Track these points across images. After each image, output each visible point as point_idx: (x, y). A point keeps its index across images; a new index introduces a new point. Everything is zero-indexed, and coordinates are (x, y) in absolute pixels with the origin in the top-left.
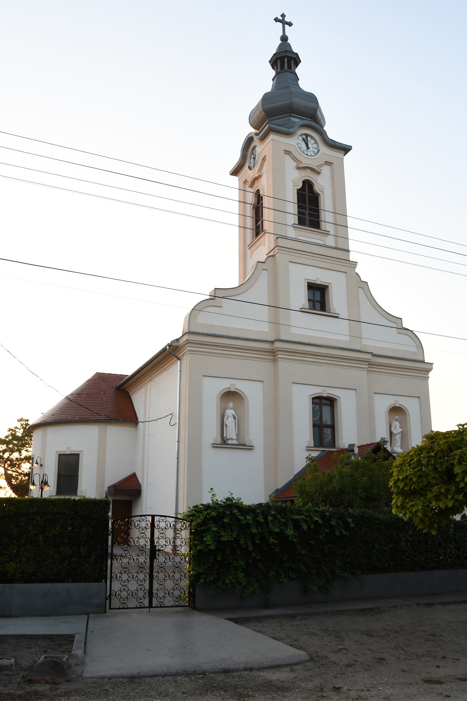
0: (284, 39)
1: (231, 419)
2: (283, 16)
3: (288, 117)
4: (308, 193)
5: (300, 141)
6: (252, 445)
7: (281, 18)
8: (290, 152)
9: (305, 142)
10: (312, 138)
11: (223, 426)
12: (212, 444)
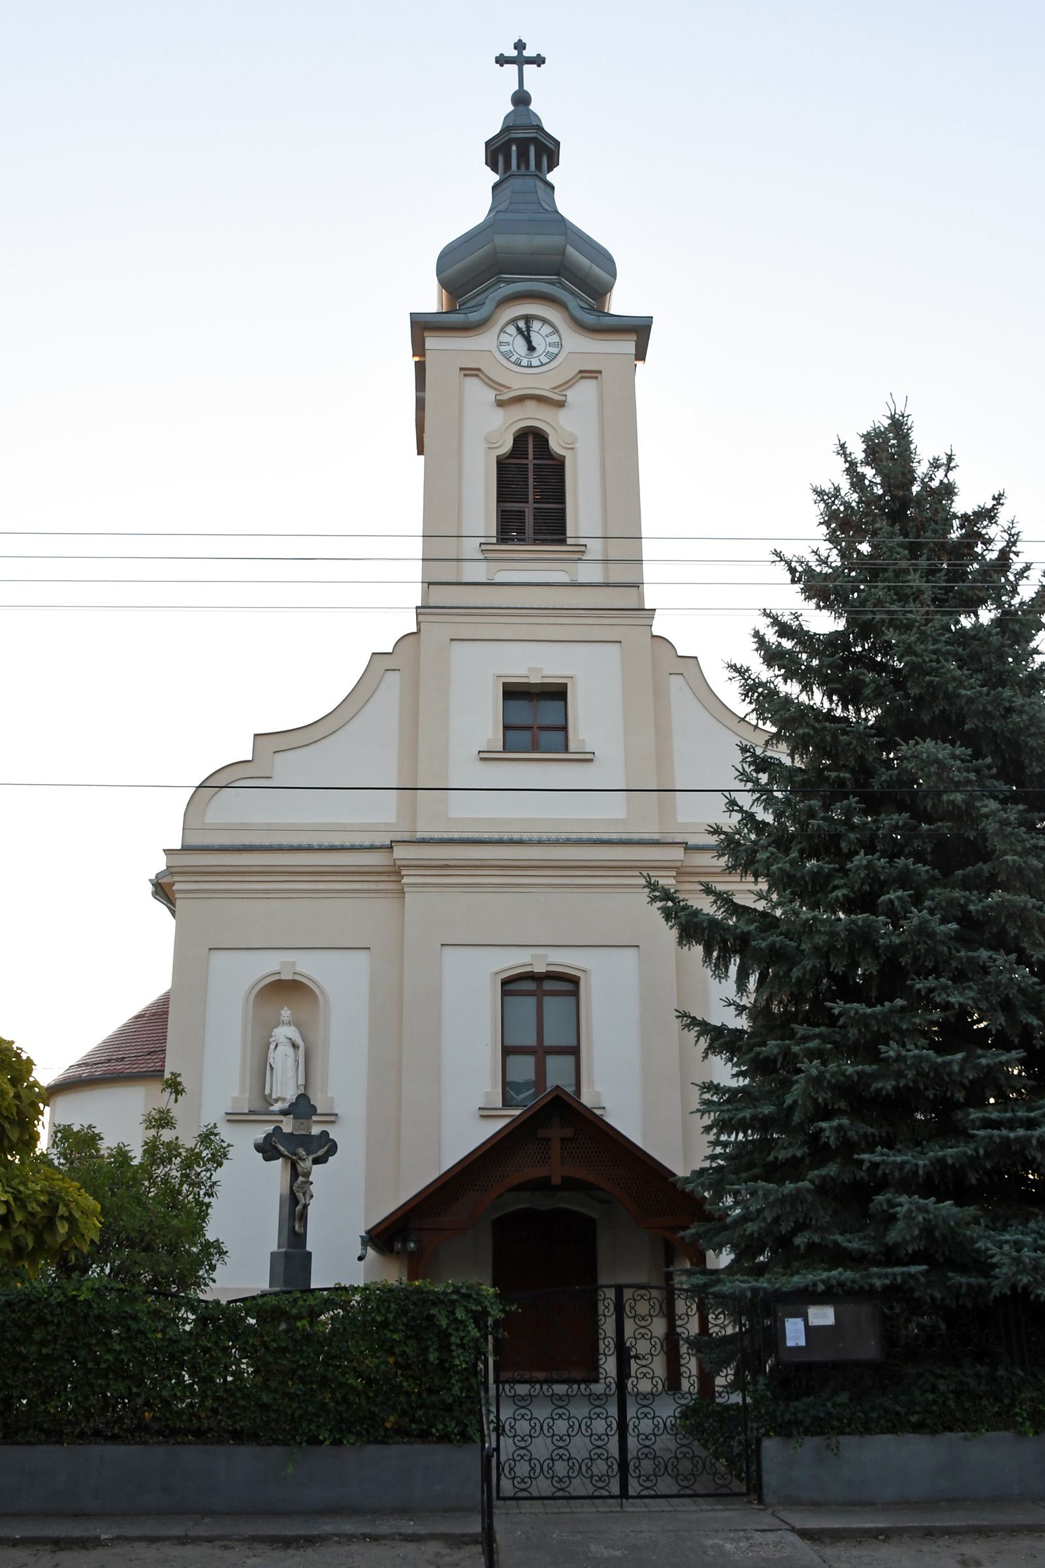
0: (521, 99)
1: (285, 1049)
2: (520, 46)
3: (494, 285)
4: (534, 458)
5: (511, 335)
6: (601, 1105)
7: (515, 53)
8: (479, 370)
9: (524, 336)
10: (544, 321)
11: (263, 1068)
12: (227, 1114)
